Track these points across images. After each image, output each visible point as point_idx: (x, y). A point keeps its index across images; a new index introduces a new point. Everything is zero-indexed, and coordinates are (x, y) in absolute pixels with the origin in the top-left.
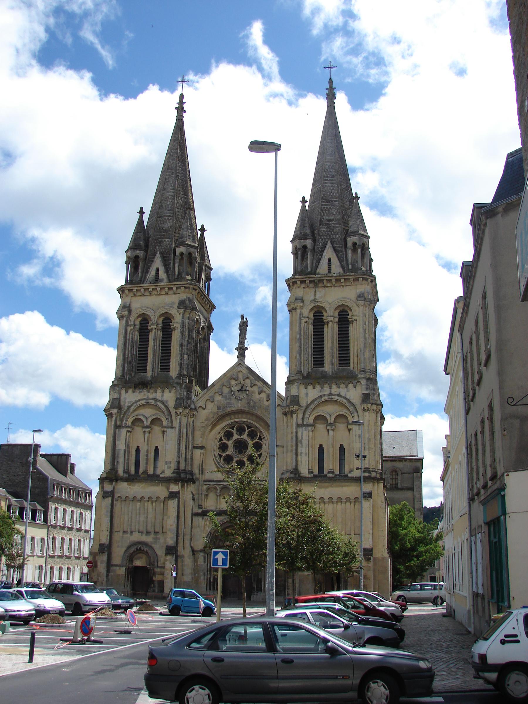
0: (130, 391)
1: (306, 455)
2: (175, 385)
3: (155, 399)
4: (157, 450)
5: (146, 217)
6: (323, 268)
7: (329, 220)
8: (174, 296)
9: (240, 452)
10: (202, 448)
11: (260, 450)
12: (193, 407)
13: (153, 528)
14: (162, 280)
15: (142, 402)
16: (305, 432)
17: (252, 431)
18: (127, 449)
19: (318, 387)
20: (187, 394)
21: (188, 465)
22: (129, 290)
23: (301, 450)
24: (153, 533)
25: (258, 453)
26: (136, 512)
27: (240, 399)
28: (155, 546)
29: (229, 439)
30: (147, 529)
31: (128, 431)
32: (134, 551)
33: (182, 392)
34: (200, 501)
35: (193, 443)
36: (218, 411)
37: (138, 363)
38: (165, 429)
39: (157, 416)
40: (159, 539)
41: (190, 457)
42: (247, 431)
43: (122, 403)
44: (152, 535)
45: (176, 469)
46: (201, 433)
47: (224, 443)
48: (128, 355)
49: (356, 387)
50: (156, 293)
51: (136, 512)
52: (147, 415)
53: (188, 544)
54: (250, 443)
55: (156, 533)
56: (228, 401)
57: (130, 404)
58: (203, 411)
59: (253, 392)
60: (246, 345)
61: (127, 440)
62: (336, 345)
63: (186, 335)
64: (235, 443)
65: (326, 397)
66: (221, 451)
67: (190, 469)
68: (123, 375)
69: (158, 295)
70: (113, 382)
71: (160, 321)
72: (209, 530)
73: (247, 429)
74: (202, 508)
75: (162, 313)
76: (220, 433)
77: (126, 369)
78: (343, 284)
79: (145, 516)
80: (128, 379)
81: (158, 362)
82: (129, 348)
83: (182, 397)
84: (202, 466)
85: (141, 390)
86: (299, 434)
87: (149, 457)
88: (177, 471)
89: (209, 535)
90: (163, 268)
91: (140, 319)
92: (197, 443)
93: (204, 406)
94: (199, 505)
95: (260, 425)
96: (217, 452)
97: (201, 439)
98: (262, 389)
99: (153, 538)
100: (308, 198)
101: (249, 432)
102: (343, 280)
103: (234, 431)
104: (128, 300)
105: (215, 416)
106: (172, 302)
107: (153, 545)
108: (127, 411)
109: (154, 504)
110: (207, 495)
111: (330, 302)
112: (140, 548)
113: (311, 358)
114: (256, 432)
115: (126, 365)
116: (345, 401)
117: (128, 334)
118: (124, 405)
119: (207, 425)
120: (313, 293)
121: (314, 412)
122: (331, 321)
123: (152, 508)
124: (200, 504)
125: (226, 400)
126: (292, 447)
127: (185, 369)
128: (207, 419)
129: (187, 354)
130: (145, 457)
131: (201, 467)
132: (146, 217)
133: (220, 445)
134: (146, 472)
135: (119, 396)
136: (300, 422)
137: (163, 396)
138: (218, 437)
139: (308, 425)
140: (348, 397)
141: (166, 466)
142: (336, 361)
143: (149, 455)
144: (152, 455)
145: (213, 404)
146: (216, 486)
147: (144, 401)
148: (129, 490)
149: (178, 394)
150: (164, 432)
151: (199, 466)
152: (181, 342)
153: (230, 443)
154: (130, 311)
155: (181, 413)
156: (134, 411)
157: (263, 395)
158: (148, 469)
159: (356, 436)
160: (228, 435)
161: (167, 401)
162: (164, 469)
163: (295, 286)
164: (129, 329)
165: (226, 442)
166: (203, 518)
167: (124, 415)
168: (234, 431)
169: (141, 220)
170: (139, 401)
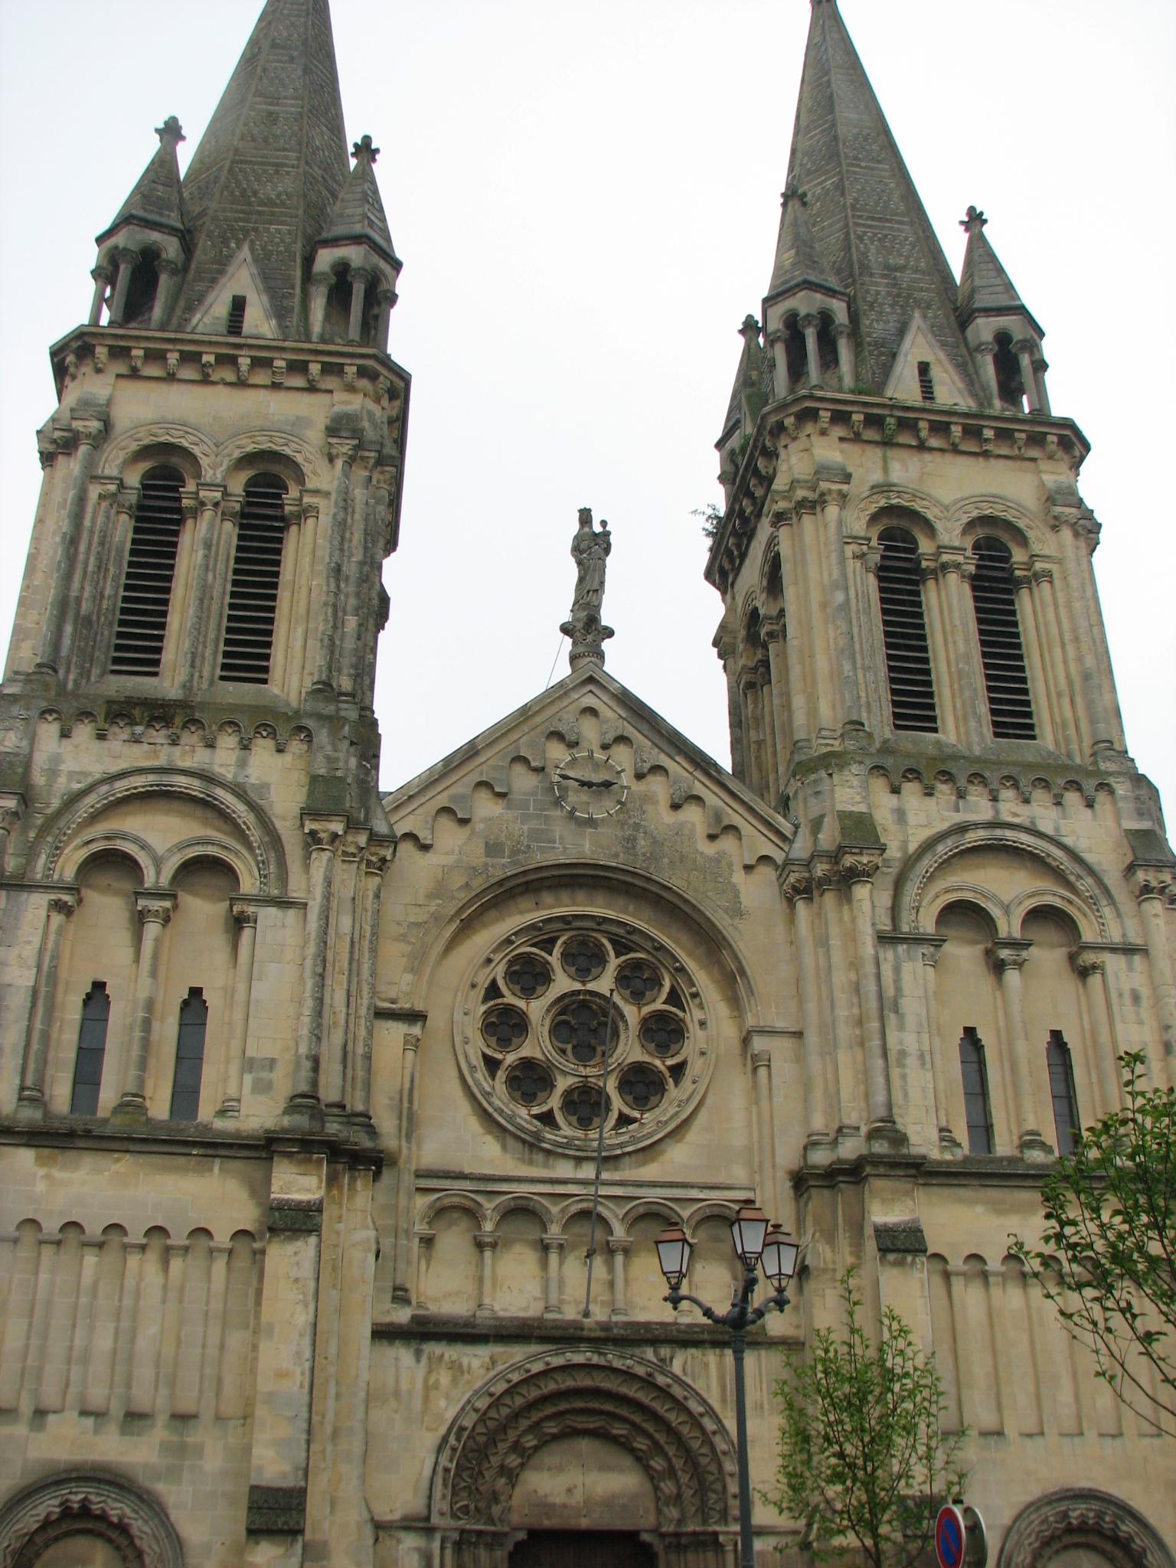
1: (923, 1064)
2: (309, 723)
4: (194, 1002)
5: (185, 156)
6: (904, 387)
8: (307, 399)
9: (585, 1052)
10: (415, 1017)
11: (674, 1047)
12: (381, 827)
13: (163, 1391)
15: (139, 782)
16: (907, 968)
17: (637, 965)
18: (43, 989)
20: (360, 766)
21: (353, 1088)
22: (111, 347)
23: (901, 1042)
24: (161, 1420)
25: (670, 1062)
26: (75, 1306)
27: (591, 822)
28: (171, 1493)
29: (528, 992)
30: (128, 1399)
31: (58, 906)
32: (47, 1524)
33: (341, 755)
34: (401, 1265)
35: (374, 992)
36: (489, 860)
37: (120, 635)
38: (250, 909)
39: (211, 850)
40: (199, 1451)
41: (360, 1050)
42: (614, 962)
43: (39, 779)
44: (159, 1432)
45: (303, 1096)
46: (407, 948)
47: (509, 1010)
48: (82, 589)
49: (1096, 806)
50: (230, 377)
51: (75, 1306)
52: (160, 845)
53: (355, 1482)
54: (632, 1014)
55: (182, 1419)
56: (534, 824)
57: (76, 786)
58: (418, 855)
59: (648, 799)
60: (606, 620)
61: (50, 945)
63: (354, 542)
64: (562, 1012)
65: (982, 833)
66: (493, 1040)
67: (360, 1107)
68: (50, 666)
69: (241, 384)
71: (238, 485)
72: (450, 1414)
73: (612, 953)
74: (407, 1301)
75: (250, 448)
76: (489, 961)
77: (67, 642)
78: (989, 447)
79: (125, 1324)
80: (70, 685)
81: (217, 639)
82: (86, 564)
83: (339, 773)
84: (411, 1102)
85: (139, 729)
87: (155, 1037)
88: (305, 1101)
89: (452, 1440)
90: (265, 299)
91: (145, 466)
92: (393, 995)
93: (425, 836)
94: (396, 1289)
95: (677, 942)
96: (477, 1046)
97: (408, 977)
98: (690, 788)
99: (166, 1448)
101: (621, 968)
102: (988, 433)
103: (554, 959)
105: (478, 884)
106: (298, 418)
107: (160, 1487)
108: (59, 813)
109: (176, 1264)
110: (428, 1242)
111: (947, 501)
112: (85, 1502)
114: (655, 970)
115: (69, 629)
116: (1058, 853)
117: (89, 509)
118: (50, 785)
119: (436, 917)
120: (880, 464)
121: (940, 884)
122: (958, 566)
123: (165, 1287)
124: (398, 1282)
125: (525, 819)
126: (860, 1022)
127: (345, 671)
128: (438, 891)
129: (356, 611)
130: (138, 1034)
131: (406, 1104)
133: (487, 1013)
134: (132, 1104)
135: (25, 743)
136: (885, 925)
137: (242, 764)
138: (483, 980)
139: (917, 940)
140: (1068, 841)
141: (248, 1079)
143: (156, 1025)
144: (168, 1029)
145: (466, 830)
146: (479, 1198)
147: (151, 778)
148: (41, 1187)
149: (320, 758)
150: (238, 923)
151: (397, 1097)
152: (336, 558)
153: (537, 1009)
154: (107, 425)
155: (335, 836)
156: (95, 817)
157: (692, 815)
158: (148, 1093)
159: (1120, 995)
161: (265, 786)
162: (232, 1092)
163: (809, 428)
164: (94, 491)
165: (521, 1004)
166: (418, 1354)
167: (44, 830)
168: (554, 959)
169: (164, 163)
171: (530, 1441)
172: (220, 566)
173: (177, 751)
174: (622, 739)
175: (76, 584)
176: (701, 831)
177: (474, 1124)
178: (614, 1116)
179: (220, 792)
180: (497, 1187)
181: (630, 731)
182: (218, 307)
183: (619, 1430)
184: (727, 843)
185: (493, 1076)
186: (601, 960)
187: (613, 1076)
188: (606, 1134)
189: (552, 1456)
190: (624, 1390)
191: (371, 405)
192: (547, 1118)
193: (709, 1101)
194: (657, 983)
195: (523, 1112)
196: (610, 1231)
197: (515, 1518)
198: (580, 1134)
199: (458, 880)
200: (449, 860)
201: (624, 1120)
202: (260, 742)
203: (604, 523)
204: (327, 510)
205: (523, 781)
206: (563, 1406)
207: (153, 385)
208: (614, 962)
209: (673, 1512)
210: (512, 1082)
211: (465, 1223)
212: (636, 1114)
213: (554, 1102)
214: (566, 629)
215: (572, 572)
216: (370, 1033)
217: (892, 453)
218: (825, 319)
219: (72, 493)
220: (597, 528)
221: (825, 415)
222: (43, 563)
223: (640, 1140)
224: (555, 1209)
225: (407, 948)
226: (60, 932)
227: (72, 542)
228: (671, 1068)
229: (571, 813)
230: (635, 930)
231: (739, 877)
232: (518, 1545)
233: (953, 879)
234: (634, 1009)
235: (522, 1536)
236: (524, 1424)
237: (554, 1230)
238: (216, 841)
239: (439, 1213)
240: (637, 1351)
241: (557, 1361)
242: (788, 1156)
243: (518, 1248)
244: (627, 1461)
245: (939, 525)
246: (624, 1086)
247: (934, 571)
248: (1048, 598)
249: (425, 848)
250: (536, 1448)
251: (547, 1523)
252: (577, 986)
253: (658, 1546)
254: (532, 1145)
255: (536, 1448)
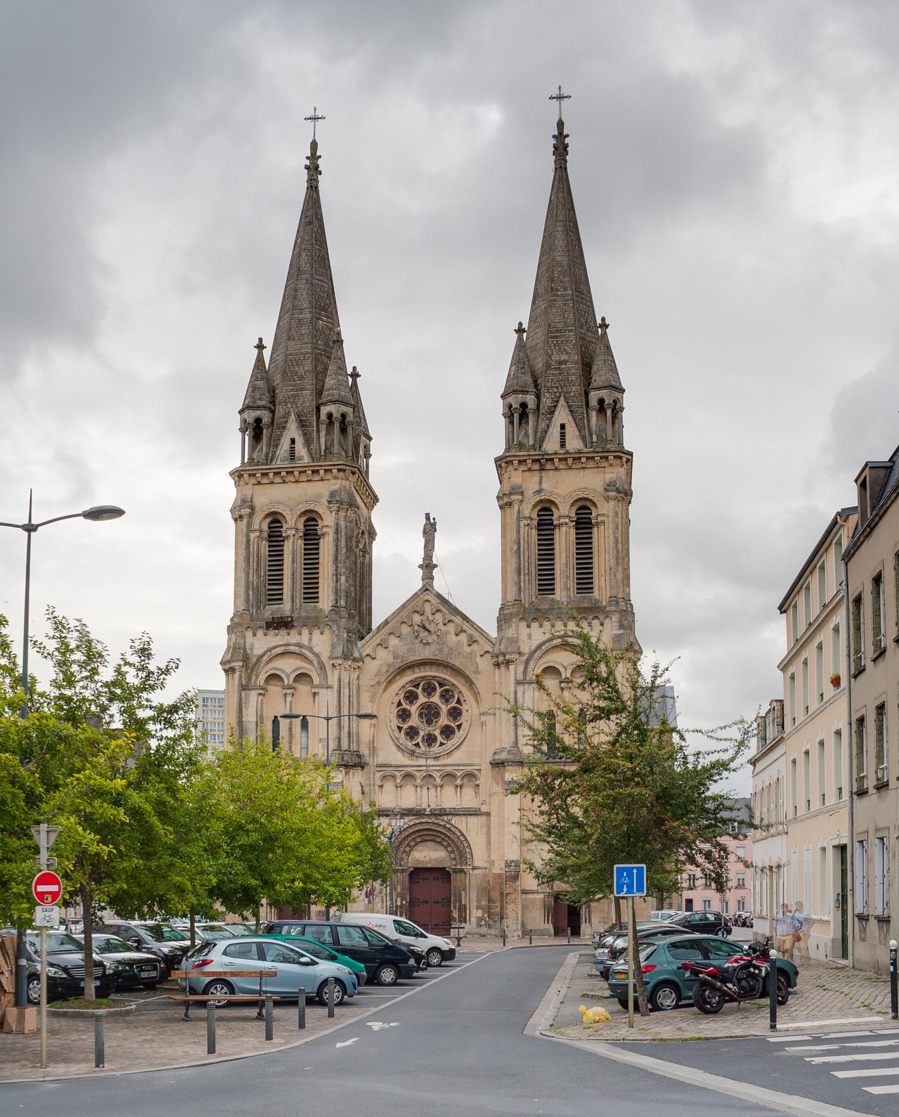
0: (260, 633)
2: (330, 623)
3: (298, 645)
5: (267, 354)
7: (560, 363)
14: (301, 458)
16: (527, 693)
17: (447, 691)
19: (547, 624)
25: (457, 724)
27: (428, 644)
29: (411, 703)
36: (395, 661)
42: (439, 690)
47: (405, 710)
52: (288, 670)
54: (444, 709)
56: (409, 646)
58: (371, 661)
62: (573, 561)
64: (422, 709)
70: (232, 619)
84: (373, 744)
86: (519, 695)
96: (395, 722)
100: (269, 343)
101: (441, 692)
103: (419, 691)
104: (248, 491)
105: (391, 670)
110: (381, 787)
113: (535, 582)
114: (453, 692)
120: (538, 479)
132: (267, 354)
133: (398, 711)
136: (520, 677)
142: (573, 585)
143: (293, 729)
147: (283, 648)
153: (414, 709)
154: (252, 508)
156: (268, 662)
157: (463, 637)
160: (411, 697)
163: (511, 468)
164: (252, 536)
165: (408, 707)
168: (419, 691)
169: (260, 359)
170: (275, 648)
171: (412, 844)
172: (298, 559)
173: (290, 637)
174: (438, 611)
175: (251, 576)
176: (465, 643)
177: (394, 749)
178: (438, 743)
179: (304, 651)
180: (401, 769)
181: (441, 607)
182: (285, 445)
183: (438, 840)
184: (475, 647)
185: (400, 731)
186: (434, 689)
187: (438, 730)
188: (435, 749)
189: (418, 848)
190: (438, 829)
191: (345, 483)
192: (417, 745)
193: (468, 737)
194: (453, 696)
195: (409, 744)
196: (436, 780)
197: (410, 865)
198: (428, 749)
199: (384, 669)
200: (382, 662)
201: (442, 744)
202: (315, 631)
203: (434, 519)
204: (331, 532)
205: (405, 630)
206: (421, 833)
207: (266, 486)
208: (439, 690)
209: (454, 863)
210: (407, 734)
211: (392, 779)
212: (445, 742)
213: (419, 740)
214: (421, 566)
215: (422, 541)
216: (358, 725)
217: (544, 473)
218: (524, 405)
219: (244, 540)
220: (432, 521)
221: (516, 462)
222: (239, 567)
223: (446, 751)
224: (418, 774)
225: (370, 694)
226: (262, 703)
227: (247, 559)
228: (457, 726)
229: (421, 641)
230: (445, 679)
231: (478, 659)
232: (412, 872)
233: (543, 660)
234: (445, 706)
235: (412, 869)
236: (410, 839)
237: (418, 781)
238: (306, 667)
239: (384, 777)
240: (441, 818)
241: (417, 821)
242: (489, 758)
243: (408, 786)
244: (442, 848)
245: (560, 506)
246: (442, 732)
247: (559, 525)
248: (602, 530)
249: (374, 659)
250: (415, 845)
251: (419, 866)
252: (427, 700)
253: (451, 871)
254: (412, 753)
255: (420, 842)
